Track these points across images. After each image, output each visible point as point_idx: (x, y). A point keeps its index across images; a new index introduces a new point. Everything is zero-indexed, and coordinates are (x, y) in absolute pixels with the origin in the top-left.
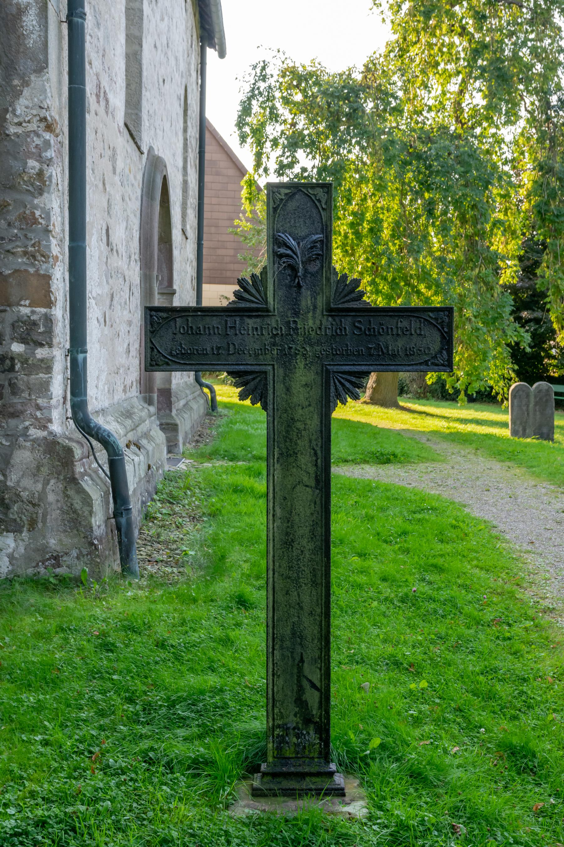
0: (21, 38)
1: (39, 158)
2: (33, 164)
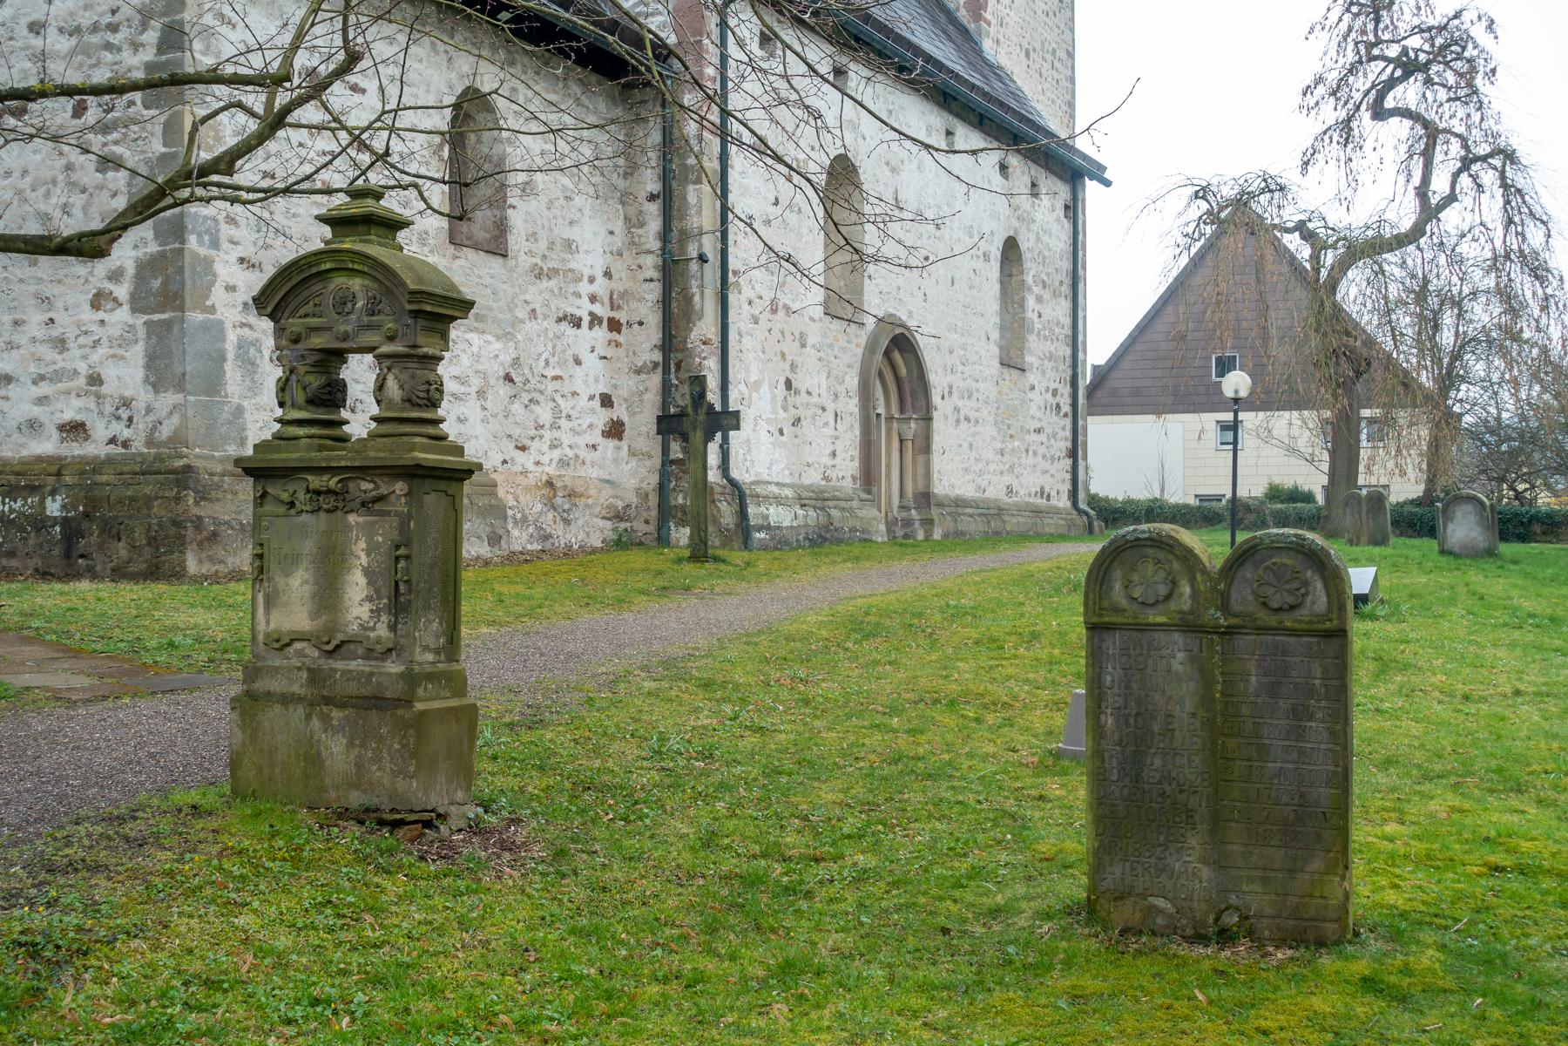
0: (693, 306)
1: (699, 357)
2: (697, 359)
